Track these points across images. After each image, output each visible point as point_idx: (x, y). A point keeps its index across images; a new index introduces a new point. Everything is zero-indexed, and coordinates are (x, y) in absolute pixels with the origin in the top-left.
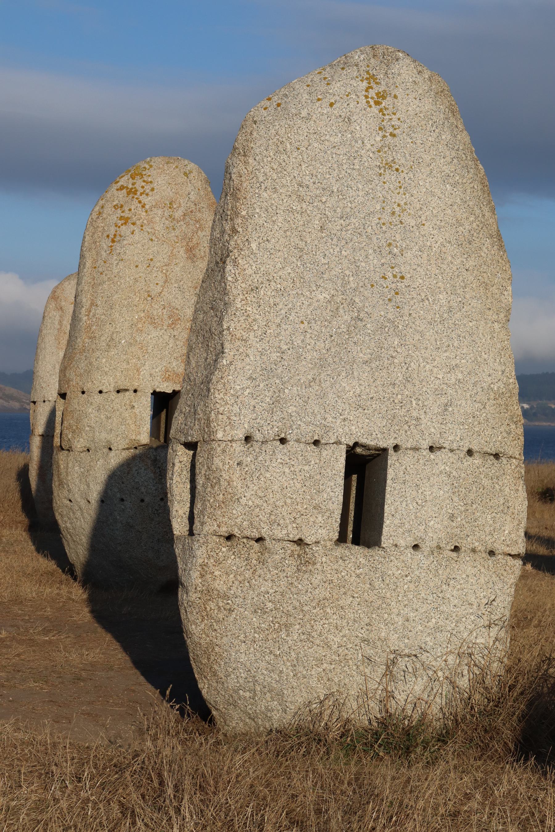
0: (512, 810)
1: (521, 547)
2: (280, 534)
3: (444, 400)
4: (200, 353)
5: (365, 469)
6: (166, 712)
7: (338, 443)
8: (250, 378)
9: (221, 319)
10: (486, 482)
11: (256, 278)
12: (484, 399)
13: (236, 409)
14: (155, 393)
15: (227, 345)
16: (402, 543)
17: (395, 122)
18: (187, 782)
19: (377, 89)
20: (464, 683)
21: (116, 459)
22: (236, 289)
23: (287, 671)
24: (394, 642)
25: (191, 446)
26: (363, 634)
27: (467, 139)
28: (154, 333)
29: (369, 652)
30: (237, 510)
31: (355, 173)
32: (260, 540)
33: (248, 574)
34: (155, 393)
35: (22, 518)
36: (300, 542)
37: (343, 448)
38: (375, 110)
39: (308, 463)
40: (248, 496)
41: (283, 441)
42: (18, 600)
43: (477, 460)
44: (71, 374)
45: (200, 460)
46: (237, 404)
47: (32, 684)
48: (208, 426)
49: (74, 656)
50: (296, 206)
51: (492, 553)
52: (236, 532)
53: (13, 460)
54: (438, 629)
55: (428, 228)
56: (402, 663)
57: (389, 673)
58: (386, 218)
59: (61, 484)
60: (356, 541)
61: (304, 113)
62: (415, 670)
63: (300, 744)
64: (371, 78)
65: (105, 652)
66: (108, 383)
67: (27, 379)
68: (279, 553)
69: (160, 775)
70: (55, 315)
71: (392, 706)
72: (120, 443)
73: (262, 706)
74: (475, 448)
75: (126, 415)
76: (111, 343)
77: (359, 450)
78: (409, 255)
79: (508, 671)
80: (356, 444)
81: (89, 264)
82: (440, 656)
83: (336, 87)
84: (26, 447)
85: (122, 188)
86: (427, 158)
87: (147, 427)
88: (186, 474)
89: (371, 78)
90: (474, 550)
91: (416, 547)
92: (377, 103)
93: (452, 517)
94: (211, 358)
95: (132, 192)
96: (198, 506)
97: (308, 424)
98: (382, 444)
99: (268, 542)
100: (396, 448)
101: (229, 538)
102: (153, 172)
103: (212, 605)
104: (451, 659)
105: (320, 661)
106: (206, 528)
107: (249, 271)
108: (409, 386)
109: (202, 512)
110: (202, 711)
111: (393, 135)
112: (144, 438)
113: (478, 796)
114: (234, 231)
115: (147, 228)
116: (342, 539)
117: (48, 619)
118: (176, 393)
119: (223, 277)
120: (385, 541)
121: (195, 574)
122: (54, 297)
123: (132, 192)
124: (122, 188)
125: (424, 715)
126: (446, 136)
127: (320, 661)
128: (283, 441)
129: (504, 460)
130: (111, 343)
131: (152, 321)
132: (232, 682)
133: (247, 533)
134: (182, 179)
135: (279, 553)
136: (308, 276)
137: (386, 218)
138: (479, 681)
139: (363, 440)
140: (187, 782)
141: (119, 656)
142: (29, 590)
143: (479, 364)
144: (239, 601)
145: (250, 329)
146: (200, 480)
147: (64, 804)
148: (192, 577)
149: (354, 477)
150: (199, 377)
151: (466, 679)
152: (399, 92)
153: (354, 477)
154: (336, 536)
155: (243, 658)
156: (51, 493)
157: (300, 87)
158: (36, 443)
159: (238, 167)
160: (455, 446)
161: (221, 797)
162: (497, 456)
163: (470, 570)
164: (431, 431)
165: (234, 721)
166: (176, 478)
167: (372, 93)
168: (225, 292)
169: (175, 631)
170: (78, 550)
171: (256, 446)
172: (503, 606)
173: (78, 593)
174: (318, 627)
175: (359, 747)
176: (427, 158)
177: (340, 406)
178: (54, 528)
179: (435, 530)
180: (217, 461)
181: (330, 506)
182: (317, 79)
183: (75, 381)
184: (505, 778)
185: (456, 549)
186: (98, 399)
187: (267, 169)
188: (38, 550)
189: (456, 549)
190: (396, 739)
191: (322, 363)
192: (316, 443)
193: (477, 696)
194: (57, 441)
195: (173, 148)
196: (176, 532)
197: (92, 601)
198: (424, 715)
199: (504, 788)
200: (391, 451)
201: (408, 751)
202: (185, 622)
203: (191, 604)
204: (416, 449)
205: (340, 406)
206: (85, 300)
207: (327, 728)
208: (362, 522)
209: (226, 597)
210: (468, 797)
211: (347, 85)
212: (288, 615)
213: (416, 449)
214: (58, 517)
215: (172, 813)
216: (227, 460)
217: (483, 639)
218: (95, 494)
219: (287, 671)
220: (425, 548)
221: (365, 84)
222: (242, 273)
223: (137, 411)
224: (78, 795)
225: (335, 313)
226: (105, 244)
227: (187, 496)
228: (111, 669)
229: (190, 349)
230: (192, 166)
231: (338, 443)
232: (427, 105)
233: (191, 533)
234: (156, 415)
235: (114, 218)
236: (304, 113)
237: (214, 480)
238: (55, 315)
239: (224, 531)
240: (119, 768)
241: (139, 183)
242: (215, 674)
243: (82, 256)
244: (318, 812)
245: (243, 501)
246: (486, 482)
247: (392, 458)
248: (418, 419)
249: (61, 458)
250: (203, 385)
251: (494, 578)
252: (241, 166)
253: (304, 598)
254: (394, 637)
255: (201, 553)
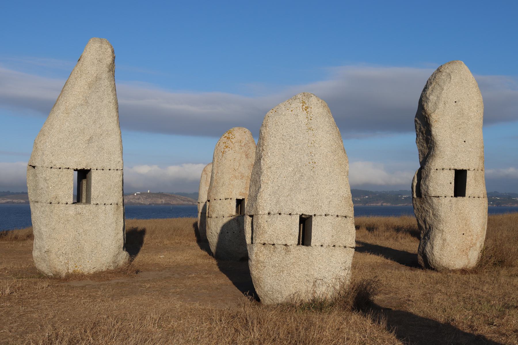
0: (356, 327)
1: (354, 245)
2: (280, 243)
3: (329, 200)
4: (253, 188)
5: (305, 222)
6: (246, 299)
7: (297, 214)
8: (269, 195)
9: (260, 177)
10: (343, 225)
11: (270, 164)
12: (341, 199)
13: (265, 204)
14: (237, 199)
15: (262, 185)
16: (317, 244)
17: (312, 116)
18: (255, 322)
19: (305, 106)
20: (338, 287)
21: (226, 220)
22: (264, 167)
23: (283, 285)
24: (316, 275)
25: (252, 216)
26: (306, 273)
27: (333, 120)
28: (236, 181)
29: (308, 278)
30: (266, 236)
31: (300, 131)
32: (273, 245)
33: (270, 255)
34: (237, 199)
35: (195, 238)
36: (286, 245)
37: (299, 216)
38: (305, 112)
39: (288, 220)
40: (270, 231)
41: (280, 214)
42: (196, 264)
43: (340, 218)
44: (211, 194)
45: (254, 220)
46: (266, 203)
47: (203, 291)
48: (257, 210)
49: (215, 282)
50: (282, 142)
51: (345, 247)
52: (266, 242)
53: (193, 220)
54: (329, 271)
55: (322, 148)
56: (318, 282)
57: (314, 285)
58: (309, 145)
59: (209, 228)
60: (303, 244)
61: (283, 114)
62: (322, 284)
63: (288, 308)
64: (304, 102)
65: (223, 281)
66: (223, 197)
67: (196, 195)
68: (280, 248)
69: (246, 319)
70: (205, 176)
71: (316, 296)
72: (227, 215)
73: (275, 296)
74: (339, 215)
75: (228, 206)
76: (223, 184)
77: (303, 216)
78: (317, 156)
79: (351, 283)
80: (302, 214)
81: (216, 160)
82: (330, 279)
83: (293, 105)
84: (197, 216)
85: (225, 137)
86: (321, 126)
87: (235, 210)
88: (250, 225)
89: (304, 102)
90: (340, 246)
91: (322, 246)
92: (306, 110)
93: (333, 236)
94: (257, 189)
95: (228, 138)
96: (254, 235)
97: (287, 208)
98: (310, 214)
99: (276, 245)
100: (315, 215)
101: (264, 244)
102: (235, 132)
103: (259, 265)
104: (333, 280)
105: (293, 282)
106: (257, 241)
107: (268, 162)
108: (318, 196)
109: (255, 237)
110: (257, 299)
111: (311, 119)
112: (234, 213)
113: (345, 323)
114: (263, 150)
115: (233, 149)
116: (299, 244)
117: (206, 270)
118: (243, 199)
119: (260, 164)
120: (312, 244)
121: (254, 256)
122: (204, 170)
123: (228, 138)
124: (225, 137)
125: (326, 298)
126: (327, 119)
127: (293, 282)
128: (280, 214)
129: (348, 218)
130: (223, 184)
131: (236, 177)
132: (266, 289)
133: (270, 243)
134: (243, 134)
135: (280, 248)
136: (286, 163)
137: (309, 145)
138: (342, 287)
139: (305, 213)
140: (255, 322)
141: (230, 282)
142: (200, 261)
143: (339, 188)
144: (267, 264)
145: (269, 180)
146: (255, 227)
147: (217, 329)
148: (253, 257)
149: (302, 225)
150: (254, 195)
151: (338, 286)
152: (312, 106)
153: (302, 225)
154: (297, 243)
155: (269, 281)
156: (206, 231)
157: (282, 106)
158: (199, 215)
159: (264, 131)
160: (333, 214)
161: (266, 326)
162: (346, 217)
163: (339, 253)
164: (325, 209)
165: (266, 301)
166: (247, 226)
167: (304, 107)
168: (261, 169)
169: (247, 273)
170: (213, 249)
171: (272, 216)
172: (349, 263)
173: (215, 262)
174: (292, 271)
175: (306, 308)
176: (321, 126)
177: (297, 203)
178: (207, 241)
179: (328, 240)
180: (260, 221)
181: (295, 234)
182: (287, 103)
183: (212, 196)
184: (353, 317)
185: (334, 246)
186: (219, 202)
187: (273, 131)
188: (201, 249)
189: (334, 246)
190: (317, 306)
191: (291, 190)
192: (290, 214)
193: (342, 292)
194: (207, 215)
195: (240, 124)
196: (247, 243)
197: (218, 264)
198: (326, 298)
199: (353, 320)
200: (313, 216)
201: (321, 309)
202: (251, 270)
203: (253, 265)
204: (321, 215)
205: (297, 203)
206: (215, 171)
207: (296, 303)
208: (305, 238)
209: (263, 262)
210: (342, 324)
211: (296, 105)
212: (283, 268)
213: (321, 215)
214: (208, 238)
215: (251, 331)
216: (262, 220)
217: (343, 274)
218: (219, 231)
219: (283, 285)
220: (325, 246)
221: (302, 104)
222: (265, 163)
223: (231, 205)
224: (221, 326)
225: (295, 174)
226: (221, 154)
227: (250, 232)
228: (227, 285)
229: (250, 186)
230: (247, 130)
231: (297, 214)
232: (321, 110)
233: (252, 243)
234: (237, 206)
235: (223, 146)
236: (283, 114)
237: (259, 227)
238: (205, 176)
239: (262, 242)
240: (233, 317)
241: (231, 135)
242: (260, 286)
243: (214, 158)
244: (297, 330)
245: (268, 233)
246: (343, 225)
247: (314, 218)
248: (321, 206)
249: (209, 220)
250: (254, 198)
251: (346, 255)
252: (265, 130)
253: (288, 262)
254: (316, 274)
255: (255, 249)
